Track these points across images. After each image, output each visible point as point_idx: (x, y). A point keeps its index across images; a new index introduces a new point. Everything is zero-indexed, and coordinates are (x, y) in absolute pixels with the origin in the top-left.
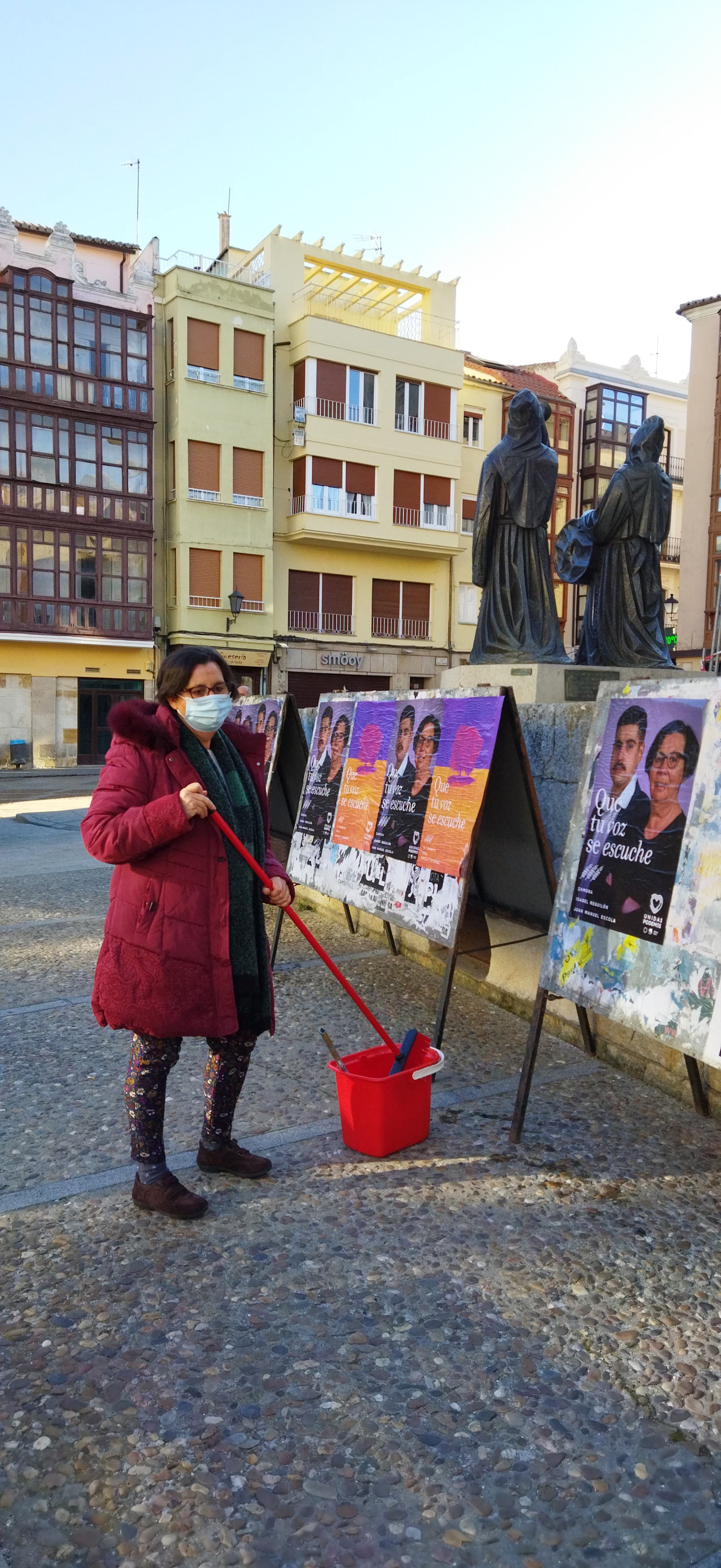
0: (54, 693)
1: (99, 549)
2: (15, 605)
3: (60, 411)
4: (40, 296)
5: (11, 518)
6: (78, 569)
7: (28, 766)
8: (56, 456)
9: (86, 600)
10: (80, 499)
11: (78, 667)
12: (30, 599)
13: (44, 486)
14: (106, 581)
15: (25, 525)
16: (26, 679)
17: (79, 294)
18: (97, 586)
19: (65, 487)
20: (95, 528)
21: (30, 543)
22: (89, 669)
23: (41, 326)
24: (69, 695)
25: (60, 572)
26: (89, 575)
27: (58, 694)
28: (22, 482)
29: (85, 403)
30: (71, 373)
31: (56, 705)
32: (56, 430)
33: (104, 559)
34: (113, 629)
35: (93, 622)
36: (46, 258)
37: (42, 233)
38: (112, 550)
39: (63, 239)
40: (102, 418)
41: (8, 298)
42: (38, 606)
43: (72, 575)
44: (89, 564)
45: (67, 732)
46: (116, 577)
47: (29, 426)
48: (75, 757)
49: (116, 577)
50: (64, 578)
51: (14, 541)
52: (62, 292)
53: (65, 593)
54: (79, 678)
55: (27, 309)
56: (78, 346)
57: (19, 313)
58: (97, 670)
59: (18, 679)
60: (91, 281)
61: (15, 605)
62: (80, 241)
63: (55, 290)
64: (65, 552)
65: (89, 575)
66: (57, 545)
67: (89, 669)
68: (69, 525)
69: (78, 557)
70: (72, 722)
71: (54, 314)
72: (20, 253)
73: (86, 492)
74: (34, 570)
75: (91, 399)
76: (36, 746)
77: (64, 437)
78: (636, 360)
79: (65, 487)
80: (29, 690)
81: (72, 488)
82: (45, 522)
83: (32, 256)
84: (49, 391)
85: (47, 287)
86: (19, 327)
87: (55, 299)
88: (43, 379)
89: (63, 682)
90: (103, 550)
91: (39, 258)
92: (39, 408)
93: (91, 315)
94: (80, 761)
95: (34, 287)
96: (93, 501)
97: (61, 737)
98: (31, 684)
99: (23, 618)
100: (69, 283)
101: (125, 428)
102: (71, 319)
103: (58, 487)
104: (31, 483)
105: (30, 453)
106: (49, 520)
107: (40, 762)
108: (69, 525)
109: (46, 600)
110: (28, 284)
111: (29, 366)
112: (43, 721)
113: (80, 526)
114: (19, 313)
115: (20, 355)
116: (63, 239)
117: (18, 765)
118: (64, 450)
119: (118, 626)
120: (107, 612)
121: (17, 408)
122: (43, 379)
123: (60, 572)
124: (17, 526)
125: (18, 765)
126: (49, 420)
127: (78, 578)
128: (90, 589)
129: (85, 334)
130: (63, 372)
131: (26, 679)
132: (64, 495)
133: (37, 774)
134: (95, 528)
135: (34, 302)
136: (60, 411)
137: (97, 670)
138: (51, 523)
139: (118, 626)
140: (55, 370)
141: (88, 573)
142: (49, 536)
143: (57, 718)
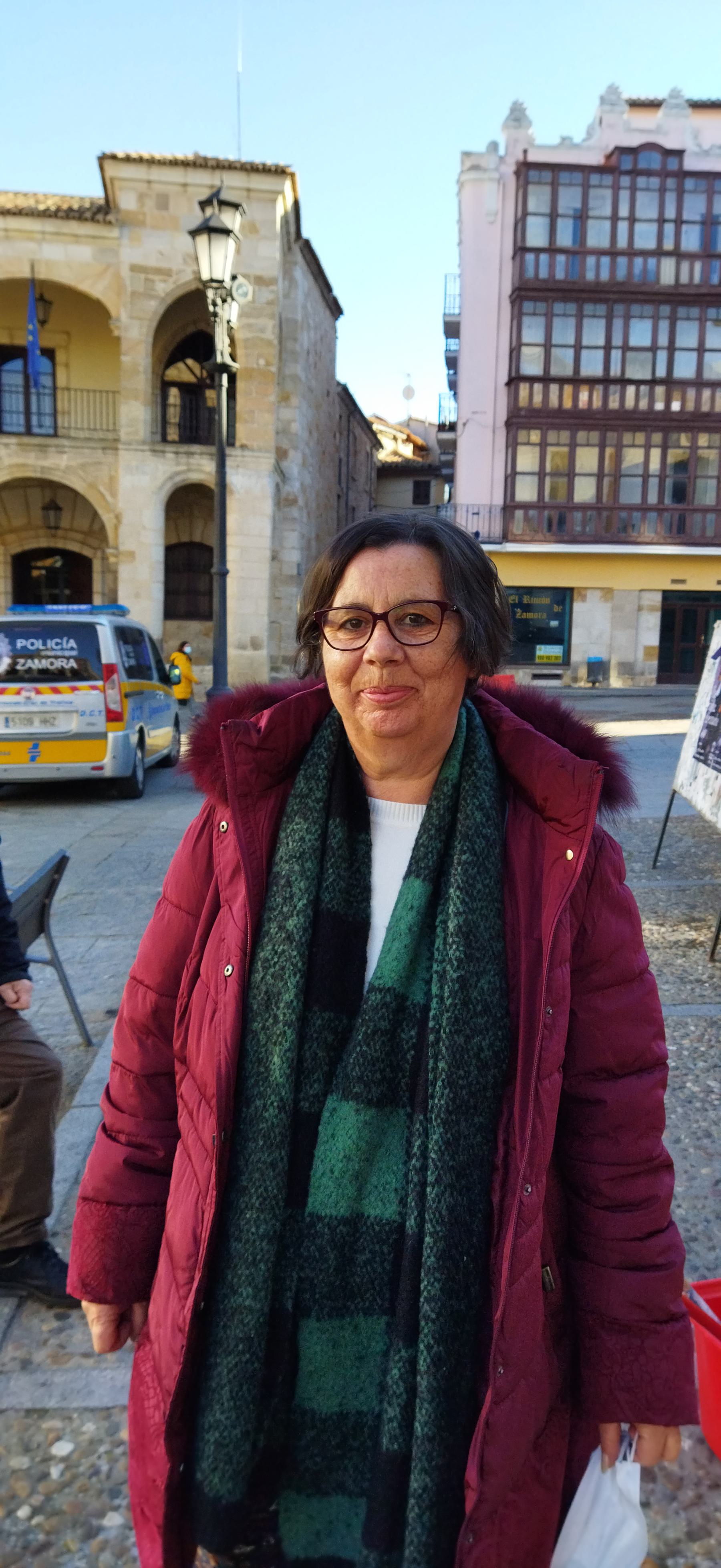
0: (636, 607)
1: (694, 447)
2: (599, 515)
3: (660, 298)
4: (648, 173)
5: (601, 422)
6: (669, 471)
7: (604, 685)
8: (653, 349)
9: (676, 506)
10: (676, 394)
11: (664, 580)
12: (616, 507)
13: (638, 383)
14: (700, 483)
15: (613, 428)
16: (608, 593)
17: (691, 164)
18: (689, 490)
19: (661, 382)
20: (691, 424)
21: (619, 447)
22: (674, 581)
23: (647, 206)
24: (652, 609)
25: (649, 476)
26: (681, 477)
27: (640, 609)
28: (615, 381)
29: (690, 284)
30: (678, 254)
31: (637, 620)
32: (656, 319)
33: (699, 459)
34: (703, 535)
35: (680, 532)
36: (658, 130)
37: (654, 105)
38: (709, 447)
39: (677, 106)
40: (709, 298)
41: (614, 182)
42: (624, 514)
43: (662, 478)
44: (681, 466)
45: (648, 650)
46: (711, 477)
47: (627, 318)
48: (654, 676)
49: (711, 477)
50: (654, 483)
51: (602, 447)
52: (672, 164)
53: (653, 498)
54: (665, 592)
55: (633, 189)
56: (687, 222)
57: (624, 195)
58: (683, 581)
59: (598, 594)
60: (706, 146)
61: (599, 515)
62: (698, 106)
63: (664, 164)
64: (656, 454)
65: (681, 477)
66: (648, 447)
67: (674, 581)
68: (663, 424)
69: (670, 460)
70: (652, 638)
71: (662, 190)
72: (629, 130)
73: (684, 384)
74: (621, 476)
75: (697, 279)
76: (613, 663)
77: (664, 325)
78: (29, 979)
79: (661, 382)
80: (609, 605)
81: (670, 383)
82: (636, 423)
83: (642, 131)
84: (651, 277)
85: (654, 161)
86: (624, 211)
87: (664, 174)
88: (645, 263)
89: (646, 595)
90: (698, 448)
91: (650, 131)
92: (640, 297)
93: (703, 184)
94: (660, 680)
95: (642, 165)
96: (691, 393)
97: (641, 654)
98: (612, 598)
99: (607, 529)
100: (679, 153)
101: (574, 429)
102: (681, 193)
103: (653, 382)
104: (624, 382)
105: (626, 348)
106: (644, 420)
107: (616, 682)
108: (663, 424)
109: (631, 508)
110: (635, 162)
111: (631, 253)
112: (623, 637)
113: (674, 424)
114: (624, 195)
115: (622, 242)
116: (677, 106)
117: (594, 683)
118: (663, 340)
119: (710, 532)
120: (698, 517)
121: (616, 301)
122: (645, 263)
123: (649, 476)
124: (607, 430)
125: (594, 683)
126: (649, 309)
127: (669, 483)
128: (680, 493)
129: (695, 207)
130: (668, 254)
131: (608, 593)
132: (660, 390)
133: (610, 693)
134: (691, 424)
135: (641, 181)
136: (660, 298)
137: (683, 581)
138: (643, 423)
139: (710, 532)
140: (659, 253)
141: (680, 476)
142: (640, 438)
143: (637, 634)
